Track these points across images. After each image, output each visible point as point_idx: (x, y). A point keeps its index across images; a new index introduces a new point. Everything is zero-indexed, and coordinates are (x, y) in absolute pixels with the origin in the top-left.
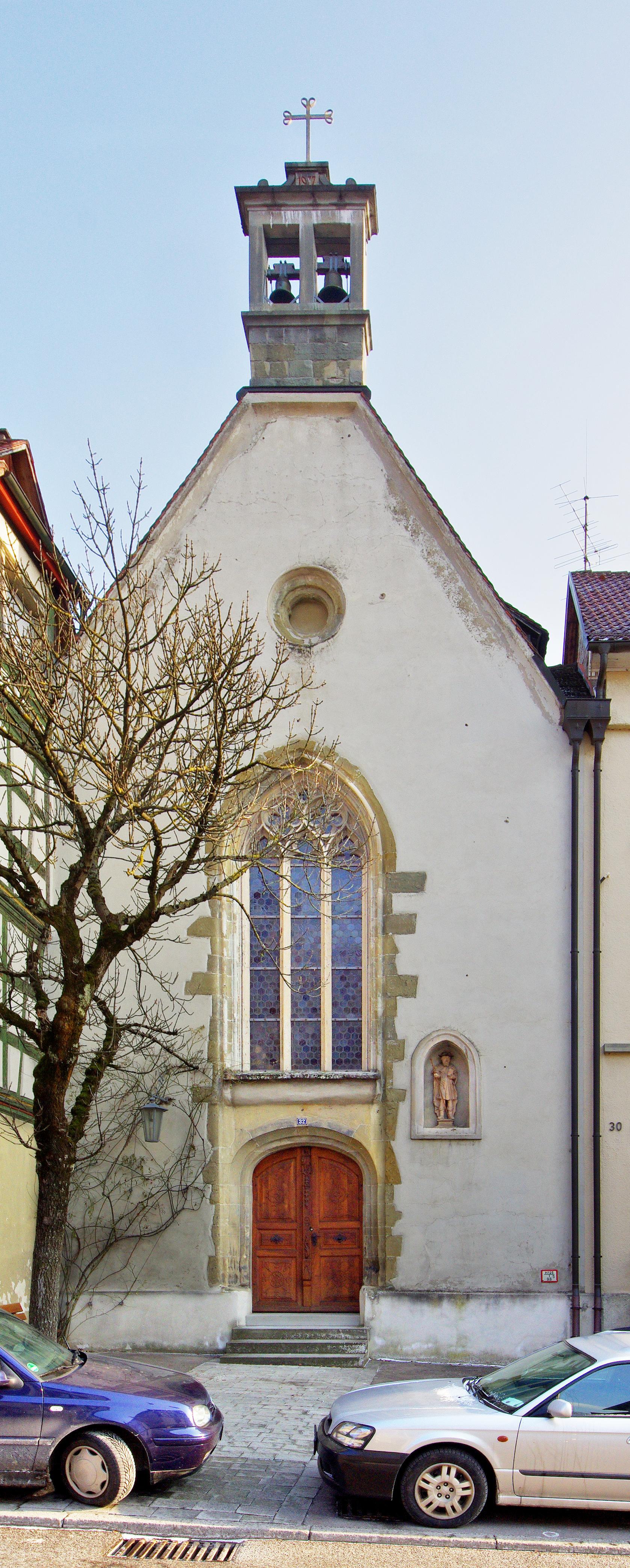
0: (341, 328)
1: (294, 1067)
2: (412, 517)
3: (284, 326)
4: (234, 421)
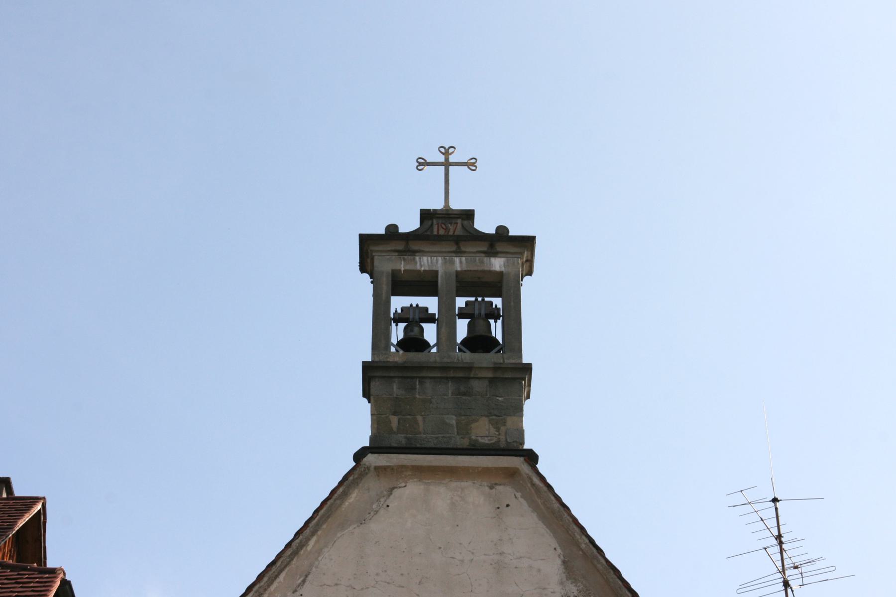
3: (416, 377)
4: (349, 487)
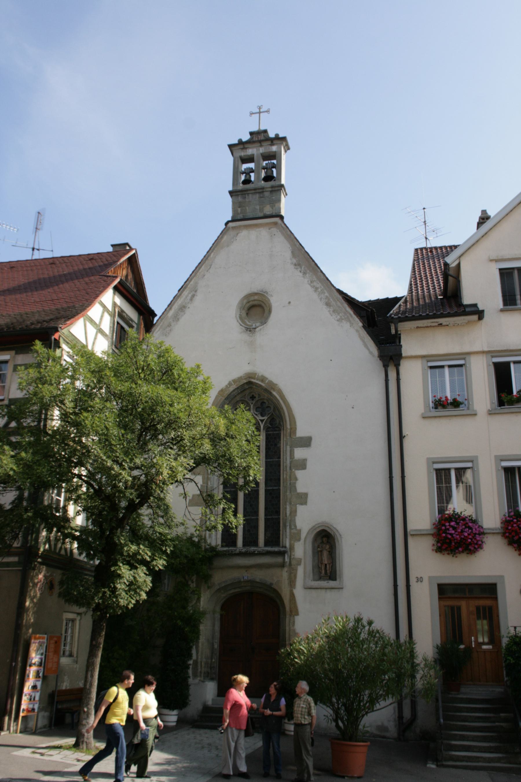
1: (244, 545)
2: (303, 267)
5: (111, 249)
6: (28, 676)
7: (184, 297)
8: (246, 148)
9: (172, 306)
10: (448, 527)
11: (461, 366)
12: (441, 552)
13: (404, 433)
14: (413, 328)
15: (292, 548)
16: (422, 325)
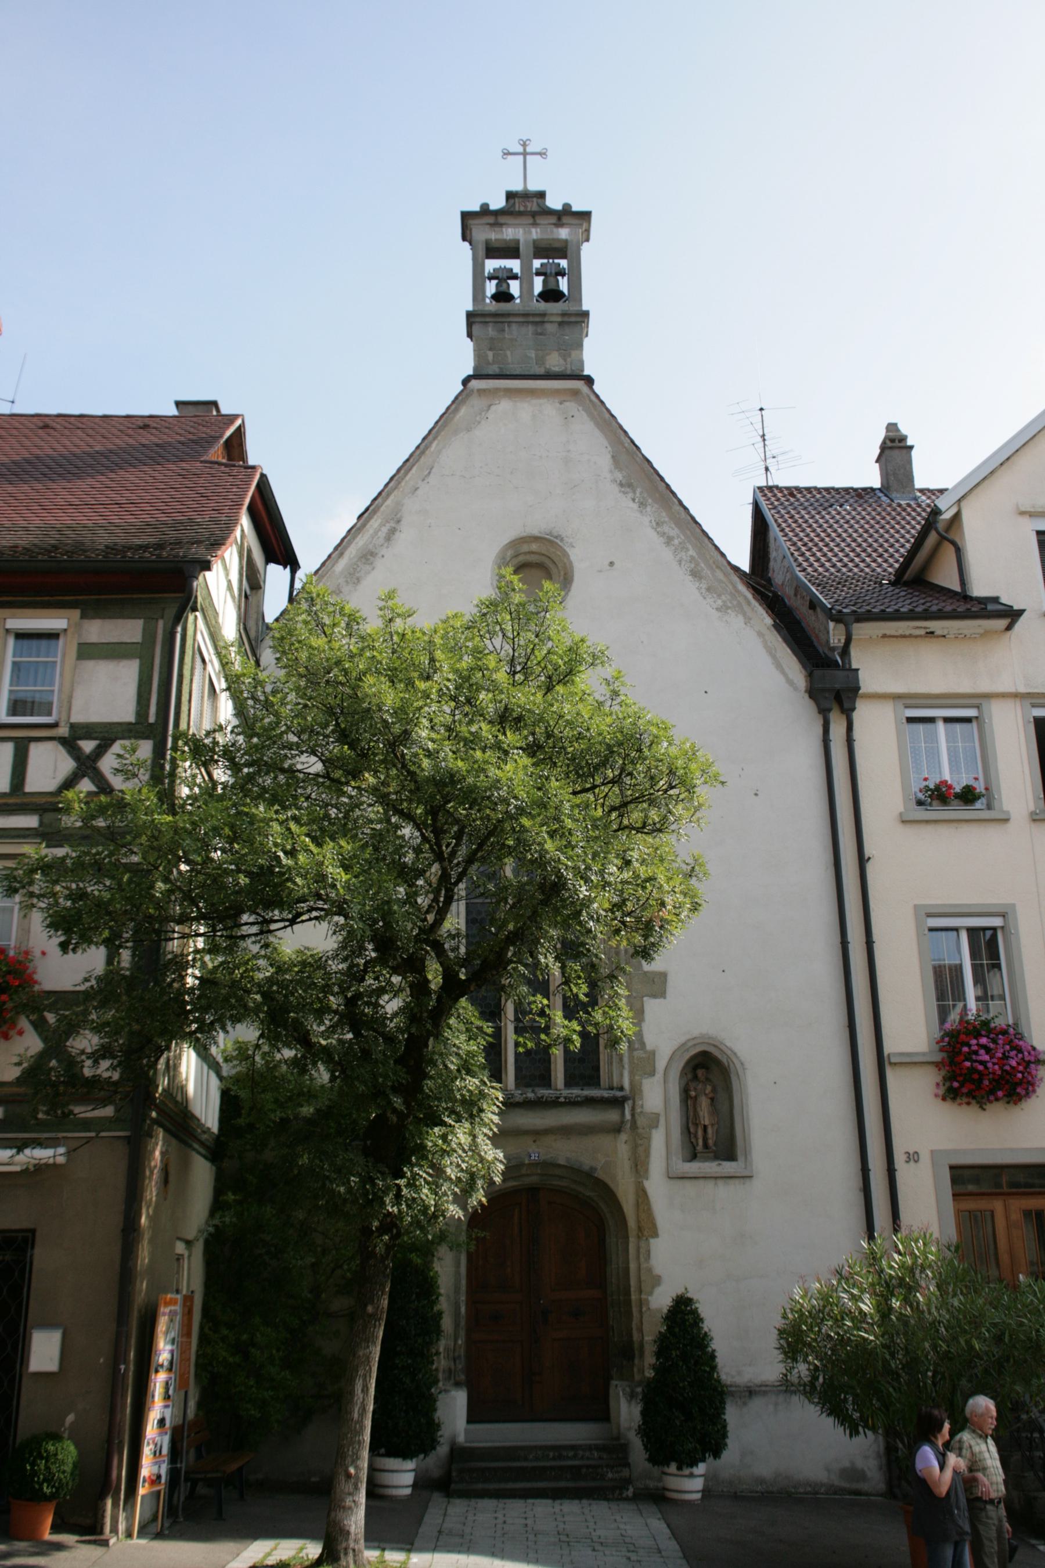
0: (561, 324)
2: (638, 490)
5: (173, 411)
6: (153, 1396)
7: (371, 531)
8: (501, 225)
9: (346, 548)
10: (975, 1048)
11: (967, 720)
12: (954, 1099)
13: (868, 851)
14: (875, 637)
15: (636, 1091)
16: (893, 633)
